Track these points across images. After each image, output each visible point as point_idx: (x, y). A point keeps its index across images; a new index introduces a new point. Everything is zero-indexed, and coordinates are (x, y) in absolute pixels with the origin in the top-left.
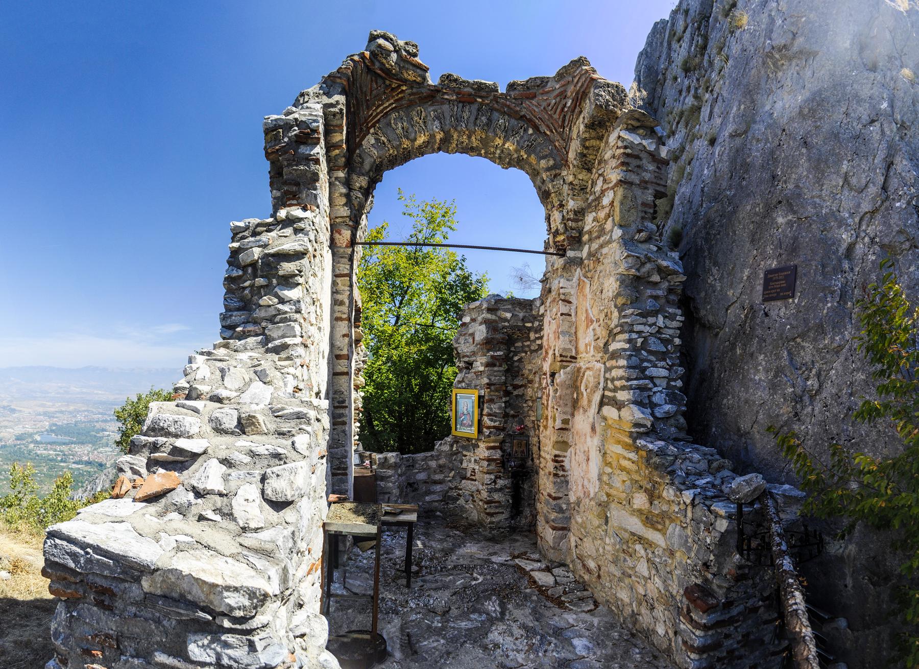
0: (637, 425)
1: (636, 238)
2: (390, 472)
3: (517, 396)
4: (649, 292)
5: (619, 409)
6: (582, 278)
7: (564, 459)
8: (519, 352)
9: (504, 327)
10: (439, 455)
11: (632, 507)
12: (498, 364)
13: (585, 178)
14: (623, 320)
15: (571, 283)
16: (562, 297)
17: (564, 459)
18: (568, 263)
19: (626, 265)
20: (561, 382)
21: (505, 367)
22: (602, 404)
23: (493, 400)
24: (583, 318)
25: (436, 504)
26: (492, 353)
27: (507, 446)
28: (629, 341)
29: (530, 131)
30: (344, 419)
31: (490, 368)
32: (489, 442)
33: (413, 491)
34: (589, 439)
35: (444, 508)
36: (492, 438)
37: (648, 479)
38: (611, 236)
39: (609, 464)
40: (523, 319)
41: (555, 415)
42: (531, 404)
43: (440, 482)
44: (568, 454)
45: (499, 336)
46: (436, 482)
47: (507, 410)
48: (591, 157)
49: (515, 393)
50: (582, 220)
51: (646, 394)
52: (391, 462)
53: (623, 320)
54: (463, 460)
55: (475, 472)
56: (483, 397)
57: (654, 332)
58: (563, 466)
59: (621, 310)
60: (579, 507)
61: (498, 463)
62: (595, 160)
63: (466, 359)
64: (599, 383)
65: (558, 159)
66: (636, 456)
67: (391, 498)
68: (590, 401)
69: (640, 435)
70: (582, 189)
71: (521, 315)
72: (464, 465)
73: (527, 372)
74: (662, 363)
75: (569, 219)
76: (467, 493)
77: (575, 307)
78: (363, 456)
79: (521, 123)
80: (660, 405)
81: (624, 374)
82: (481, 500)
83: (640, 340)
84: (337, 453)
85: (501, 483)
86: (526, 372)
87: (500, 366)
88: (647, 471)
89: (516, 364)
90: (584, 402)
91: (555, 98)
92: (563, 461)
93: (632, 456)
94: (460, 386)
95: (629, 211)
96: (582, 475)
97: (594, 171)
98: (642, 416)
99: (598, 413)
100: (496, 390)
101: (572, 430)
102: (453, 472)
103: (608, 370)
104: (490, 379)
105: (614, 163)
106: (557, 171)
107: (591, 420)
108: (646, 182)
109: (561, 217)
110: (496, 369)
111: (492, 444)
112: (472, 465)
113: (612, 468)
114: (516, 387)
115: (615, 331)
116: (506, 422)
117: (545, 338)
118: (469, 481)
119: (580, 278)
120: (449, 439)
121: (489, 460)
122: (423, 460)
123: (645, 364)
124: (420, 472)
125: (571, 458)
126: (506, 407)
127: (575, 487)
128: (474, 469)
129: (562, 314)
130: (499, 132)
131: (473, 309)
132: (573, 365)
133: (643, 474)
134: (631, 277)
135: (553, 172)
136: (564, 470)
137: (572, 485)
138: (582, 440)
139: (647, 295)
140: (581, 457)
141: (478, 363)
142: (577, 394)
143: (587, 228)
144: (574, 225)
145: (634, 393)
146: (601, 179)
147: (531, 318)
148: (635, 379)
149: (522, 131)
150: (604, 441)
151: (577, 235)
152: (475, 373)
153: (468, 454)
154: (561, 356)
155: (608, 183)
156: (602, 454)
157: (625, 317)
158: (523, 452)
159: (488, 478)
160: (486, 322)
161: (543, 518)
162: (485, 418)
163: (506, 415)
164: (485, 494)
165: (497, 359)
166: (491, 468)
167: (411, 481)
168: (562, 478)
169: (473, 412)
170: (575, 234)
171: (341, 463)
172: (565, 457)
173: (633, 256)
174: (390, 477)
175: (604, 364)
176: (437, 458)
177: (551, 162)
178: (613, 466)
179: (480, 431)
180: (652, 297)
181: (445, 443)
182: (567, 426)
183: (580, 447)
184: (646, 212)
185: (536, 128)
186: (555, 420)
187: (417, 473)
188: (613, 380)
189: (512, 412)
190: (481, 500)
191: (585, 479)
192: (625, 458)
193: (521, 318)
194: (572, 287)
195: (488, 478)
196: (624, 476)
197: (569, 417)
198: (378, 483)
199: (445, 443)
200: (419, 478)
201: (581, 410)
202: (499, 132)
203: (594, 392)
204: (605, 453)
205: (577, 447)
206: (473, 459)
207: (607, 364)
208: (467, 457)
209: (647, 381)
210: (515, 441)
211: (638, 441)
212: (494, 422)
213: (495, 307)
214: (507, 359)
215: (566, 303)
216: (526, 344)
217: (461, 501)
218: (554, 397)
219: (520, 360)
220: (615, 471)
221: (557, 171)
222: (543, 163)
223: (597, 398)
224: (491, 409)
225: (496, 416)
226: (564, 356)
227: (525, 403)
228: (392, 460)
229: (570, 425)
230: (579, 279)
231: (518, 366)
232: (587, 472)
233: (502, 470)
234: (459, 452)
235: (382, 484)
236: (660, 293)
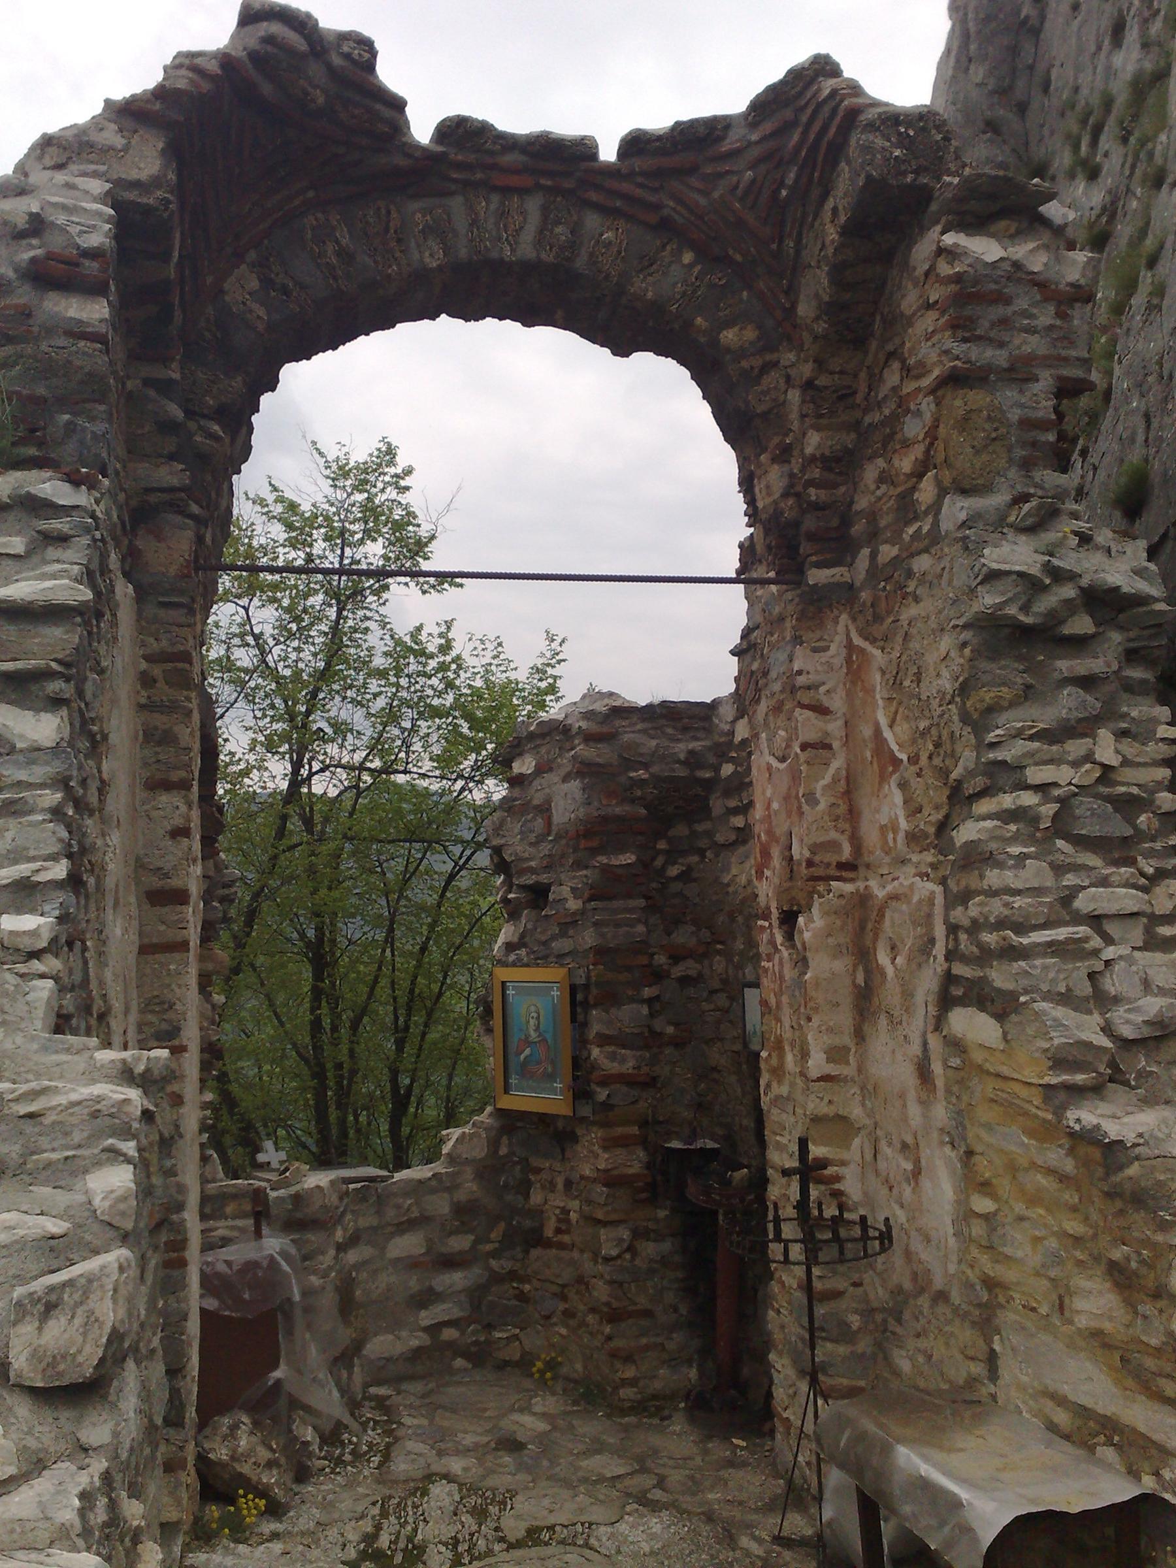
1: (1012, 519)
6: (857, 641)
11: (1070, 1322)
15: (824, 657)
22: (946, 1002)
24: (868, 754)
26: (603, 859)
38: (936, 524)
39: (985, 1187)
49: (678, 971)
57: (1086, 782)
60: (899, 1321)
62: (873, 315)
63: (529, 880)
64: (932, 941)
68: (908, 994)
82: (593, 1310)
89: (676, 887)
90: (890, 994)
91: (753, 166)
92: (838, 1178)
94: (512, 957)
97: (874, 345)
105: (929, 321)
106: (769, 357)
107: (915, 1049)
115: (969, 789)
117: (758, 813)
119: (849, 640)
129: (804, 747)
139: (1057, 676)
141: (565, 891)
143: (862, 503)
146: (896, 365)
155: (918, 377)
160: (585, 770)
161: (786, 1361)
172: (843, 1163)
175: (943, 881)
179: (580, 1093)
184: (1034, 444)
186: (804, 1055)
188: (975, 927)
195: (610, 1241)
201: (883, 1021)
206: (560, 1182)
207: (951, 883)
208: (544, 1175)
209: (1082, 930)
216: (700, 828)
221: (769, 357)
223: (927, 983)
230: (850, 646)
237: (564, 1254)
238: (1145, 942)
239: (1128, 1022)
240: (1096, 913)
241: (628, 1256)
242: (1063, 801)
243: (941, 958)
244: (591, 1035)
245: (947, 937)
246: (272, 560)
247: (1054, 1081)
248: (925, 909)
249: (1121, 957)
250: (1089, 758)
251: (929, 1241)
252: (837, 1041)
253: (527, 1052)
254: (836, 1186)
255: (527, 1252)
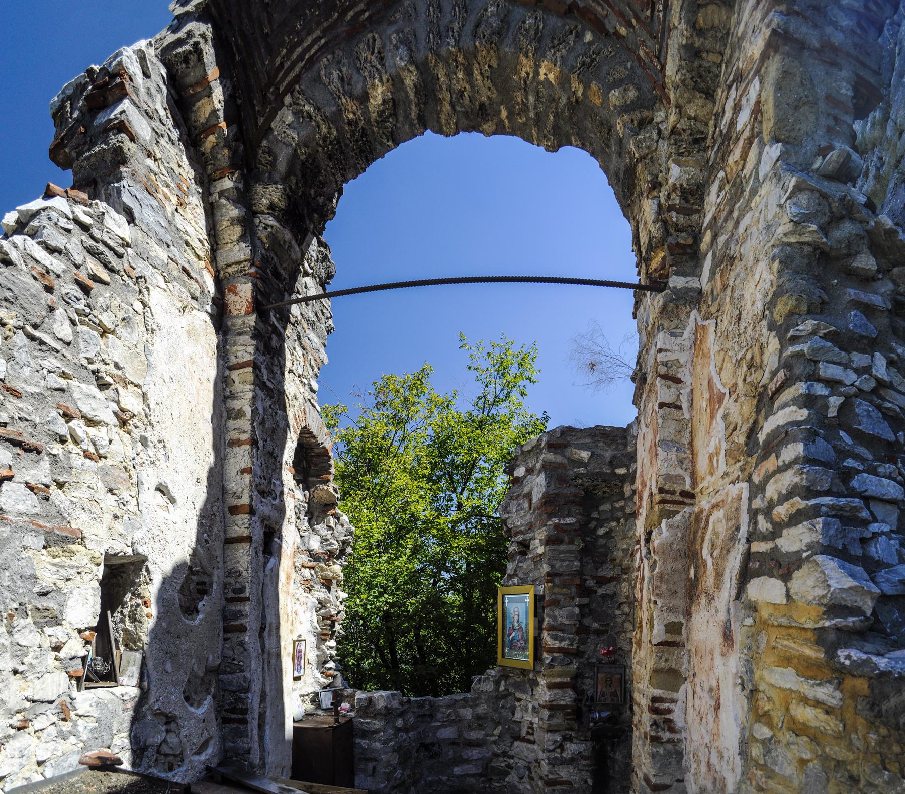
0: (834, 609)
1: (816, 166)
2: (377, 724)
3: (604, 597)
4: (851, 293)
5: (786, 577)
7: (672, 706)
8: (607, 520)
9: (578, 476)
10: (478, 698)
12: (566, 539)
13: (701, 113)
14: (791, 350)
15: (679, 340)
16: (662, 370)
17: (672, 706)
18: (672, 300)
19: (795, 210)
20: (662, 545)
21: (579, 544)
22: (745, 576)
23: (559, 602)
24: (704, 405)
25: (473, 780)
27: (587, 685)
28: (808, 401)
29: (588, 37)
30: (243, 621)
31: (553, 547)
32: (552, 676)
33: (431, 757)
34: (718, 660)
35: (485, 788)
36: (557, 668)
37: (877, 759)
39: (764, 717)
40: (611, 462)
41: (652, 616)
42: (627, 610)
43: (478, 744)
44: (680, 695)
45: (567, 491)
46: (471, 744)
47: (587, 621)
48: (713, 58)
49: (601, 591)
50: (698, 211)
51: (855, 533)
52: (379, 707)
53: (791, 350)
54: (515, 707)
55: (532, 728)
56: (543, 597)
58: (671, 721)
59: (780, 330)
61: (568, 714)
63: (520, 538)
64: (738, 528)
65: (646, 86)
66: (838, 695)
67: (378, 769)
68: (719, 575)
69: (846, 637)
70: (696, 141)
71: (608, 454)
72: (518, 716)
73: (620, 554)
74: (888, 467)
75: (670, 208)
76: (522, 763)
77: (688, 390)
78: (342, 696)
79: (571, 24)
80: (888, 566)
81: (797, 479)
82: (541, 778)
83: (835, 402)
84: (230, 683)
85: (572, 748)
86: (619, 554)
87: (571, 542)
88: (873, 737)
89: (602, 541)
90: (709, 580)
92: (669, 711)
93: (825, 693)
95: (797, 108)
96: (707, 740)
98: (849, 583)
99: (738, 597)
100: (564, 585)
101: (688, 646)
102: (500, 728)
103: (757, 490)
104: (552, 566)
106: (646, 113)
107: (722, 616)
108: (835, 50)
109: (655, 207)
110: (563, 547)
111: (558, 680)
112: (528, 717)
113: (770, 725)
114: (602, 581)
116: (583, 642)
118: (525, 744)
120: (493, 673)
121: (552, 707)
122: (448, 707)
123: (850, 463)
124: (445, 727)
125: (685, 703)
126: (582, 615)
127: (694, 766)
128: (532, 723)
129: (662, 405)
130: (524, 42)
131: (529, 451)
132: (687, 509)
133: (858, 743)
134: (807, 249)
135: (637, 115)
136: (672, 730)
137: (689, 760)
138: (707, 665)
139: (847, 298)
140: (704, 702)
141: (537, 541)
142: (696, 568)
144: (682, 220)
145: (826, 525)
147: (625, 460)
148: (827, 493)
149: (571, 38)
150: (751, 662)
151: (690, 241)
152: (533, 559)
153: (523, 696)
154: (661, 490)
156: (746, 692)
157: (794, 340)
158: (614, 694)
159: (549, 739)
160: (547, 467)
162: (545, 634)
163: (582, 630)
164: (545, 767)
165: (565, 531)
166: (555, 721)
167: (428, 741)
168: (670, 747)
169: (527, 625)
170: (684, 239)
171: (239, 700)
172: (673, 701)
173: (813, 190)
174: (377, 731)
176: (474, 704)
177: (632, 94)
178: (775, 720)
179: (537, 658)
180: (857, 304)
181: (487, 679)
182: (676, 638)
183: (704, 680)
185: (599, 27)
186: (652, 627)
187: (439, 727)
189: (595, 625)
190: (541, 778)
191: (714, 752)
192: (805, 700)
193: (608, 459)
194: (682, 349)
195: (549, 739)
196: (803, 749)
197: (681, 619)
198: (358, 740)
199: (485, 680)
200: (443, 736)
201: (703, 600)
202: (524, 42)
203: (728, 551)
204: (754, 691)
205: (697, 680)
206: (530, 706)
208: (522, 703)
209: (857, 502)
210: (600, 676)
211: (842, 653)
212: (560, 641)
213: (561, 441)
214: (584, 530)
215: (669, 383)
216: (617, 505)
217: (513, 778)
218: (651, 579)
219: (609, 534)
220: (780, 735)
221: (646, 113)
222: (615, 96)
223: (734, 562)
224: (554, 618)
225: (563, 631)
226: (667, 492)
227: (619, 608)
228: (381, 704)
229: (684, 635)
231: (605, 546)
232: (716, 735)
233: (576, 726)
234: (510, 694)
235: (364, 743)
236: (876, 300)
237: (530, 746)
238: (898, 528)
239: (888, 580)
240: (867, 494)
241: (559, 751)
242: (848, 397)
243: (743, 541)
244: (545, 625)
245: (750, 522)
246: (206, 40)
247: (827, 624)
248: (735, 505)
249: (883, 533)
250: (866, 370)
251: (722, 758)
252: (673, 618)
253: (513, 635)
254: (667, 716)
255: (512, 743)
